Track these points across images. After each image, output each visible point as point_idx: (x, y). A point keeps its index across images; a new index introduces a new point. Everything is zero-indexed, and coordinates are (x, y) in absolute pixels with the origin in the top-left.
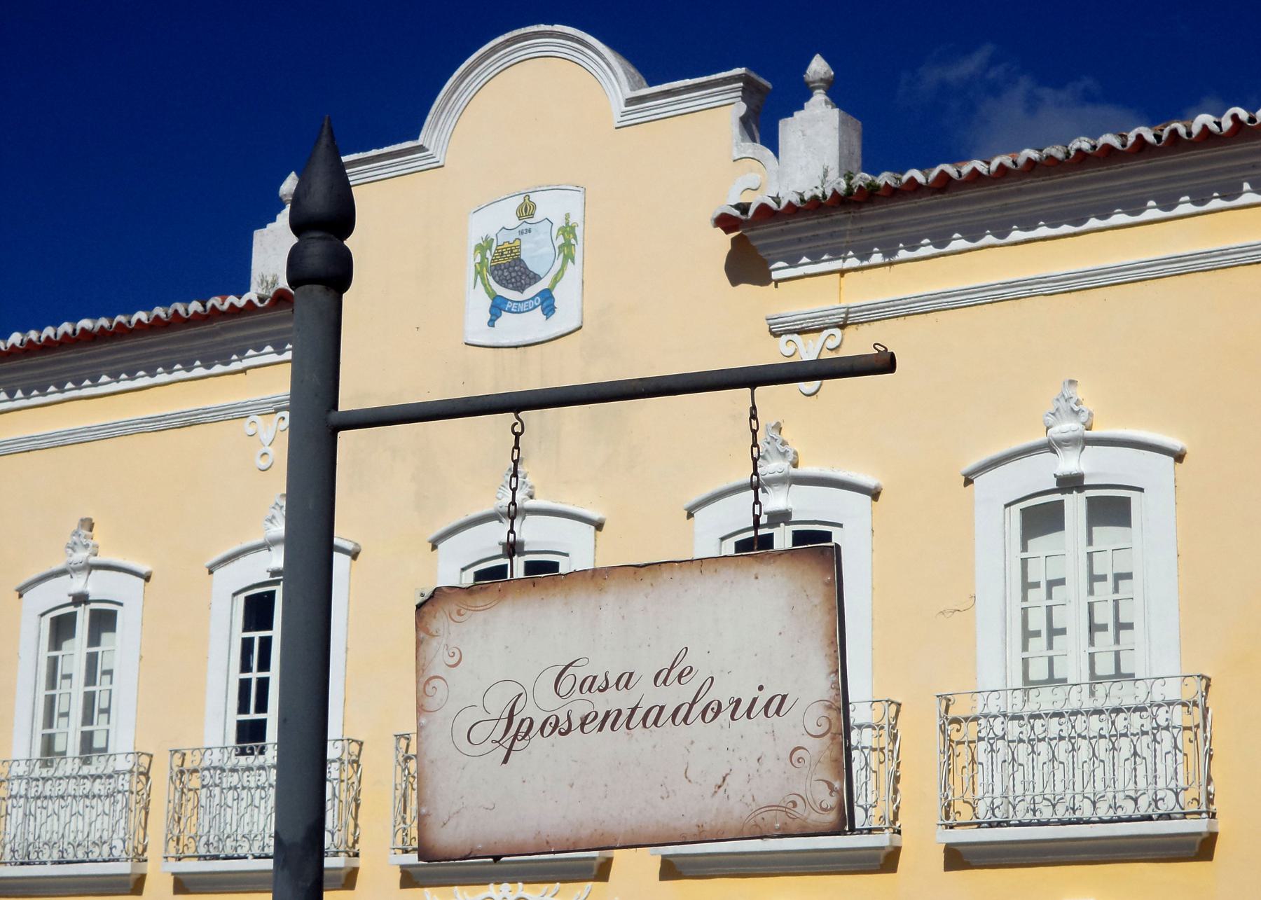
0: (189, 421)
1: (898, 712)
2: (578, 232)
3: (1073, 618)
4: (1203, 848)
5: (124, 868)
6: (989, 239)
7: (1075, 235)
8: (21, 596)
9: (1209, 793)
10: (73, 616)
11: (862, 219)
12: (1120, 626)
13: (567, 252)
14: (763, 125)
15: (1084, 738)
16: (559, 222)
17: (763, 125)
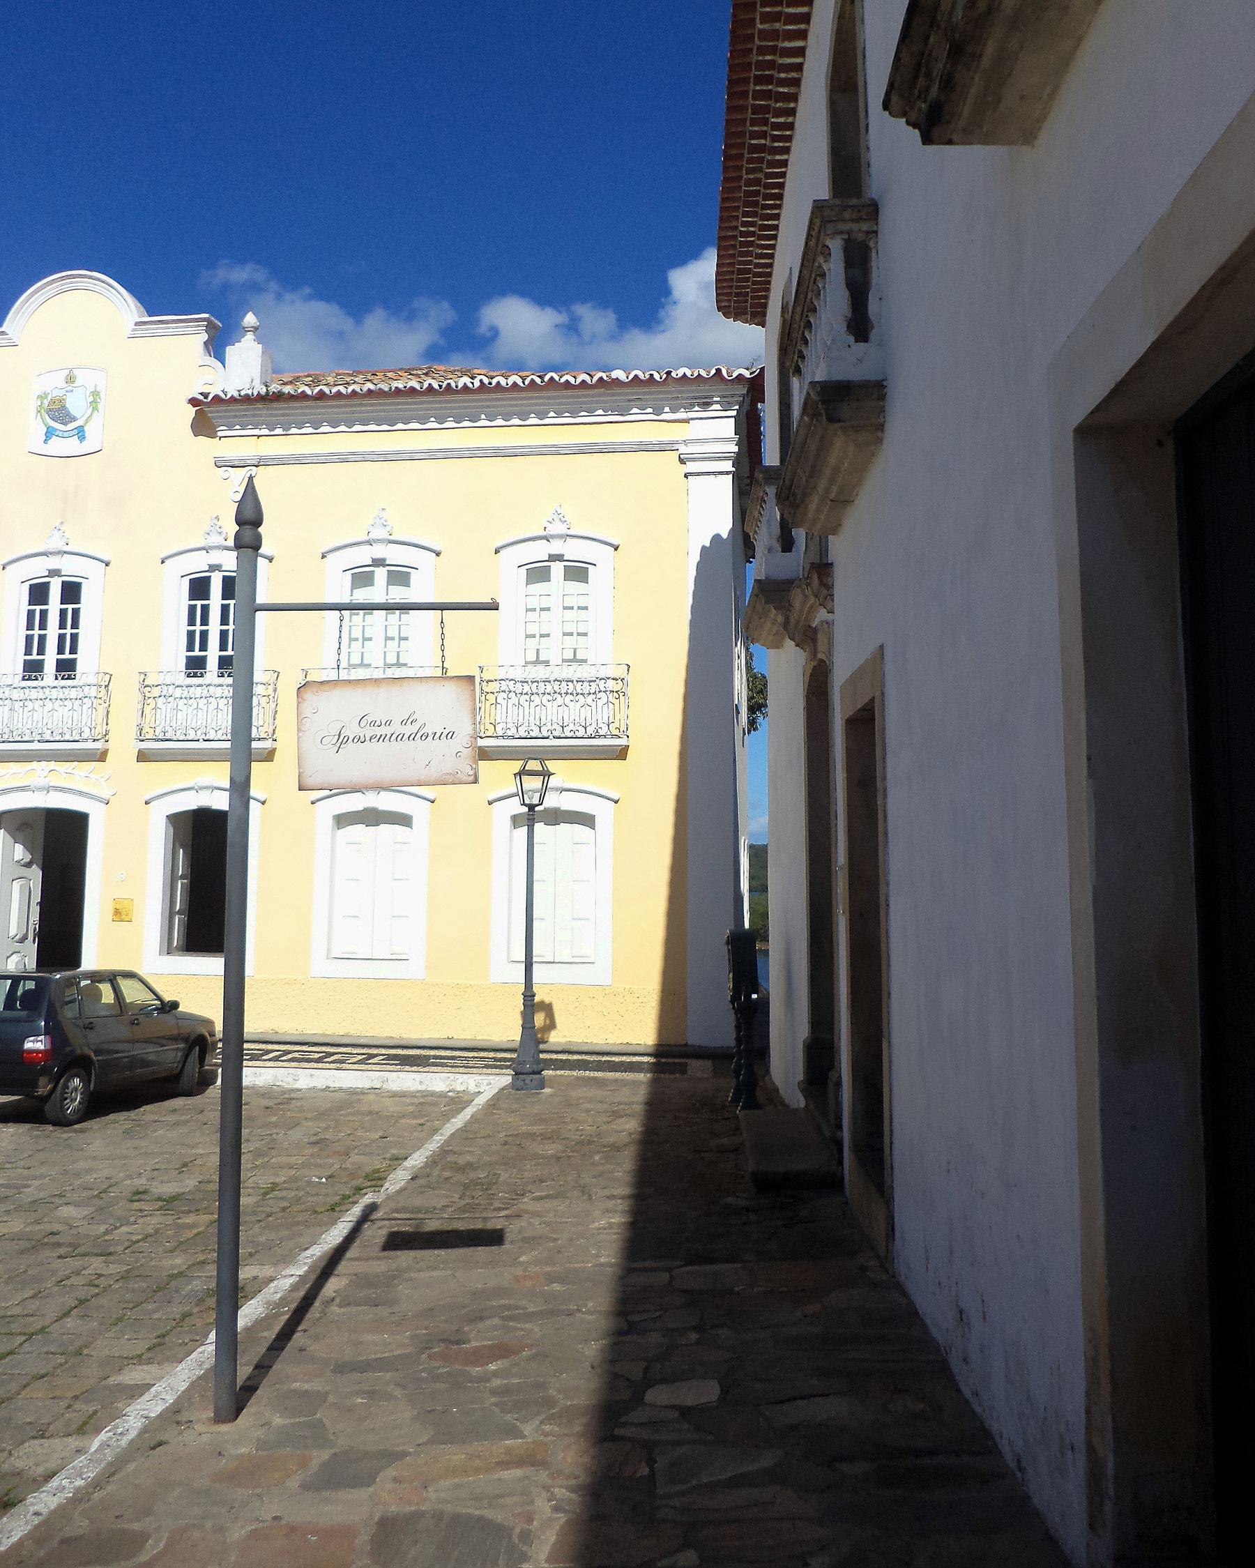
2: (102, 395)
4: (102, 756)
11: (272, 409)
12: (365, 639)
13: (94, 405)
14: (217, 346)
17: (217, 346)
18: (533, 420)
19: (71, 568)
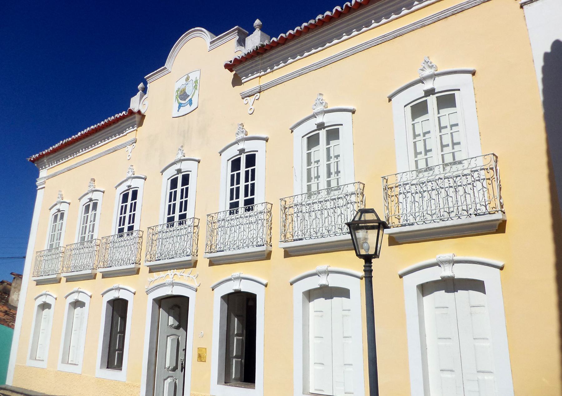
0: (115, 150)
1: (364, 187)
3: (433, 142)
4: (499, 227)
5: (89, 271)
6: (299, 57)
7: (323, 50)
8: (292, 132)
9: (501, 203)
10: (240, 159)
11: (264, 58)
13: (195, 87)
15: (442, 188)
16: (194, 80)
18: (405, 11)
19: (249, 146)
